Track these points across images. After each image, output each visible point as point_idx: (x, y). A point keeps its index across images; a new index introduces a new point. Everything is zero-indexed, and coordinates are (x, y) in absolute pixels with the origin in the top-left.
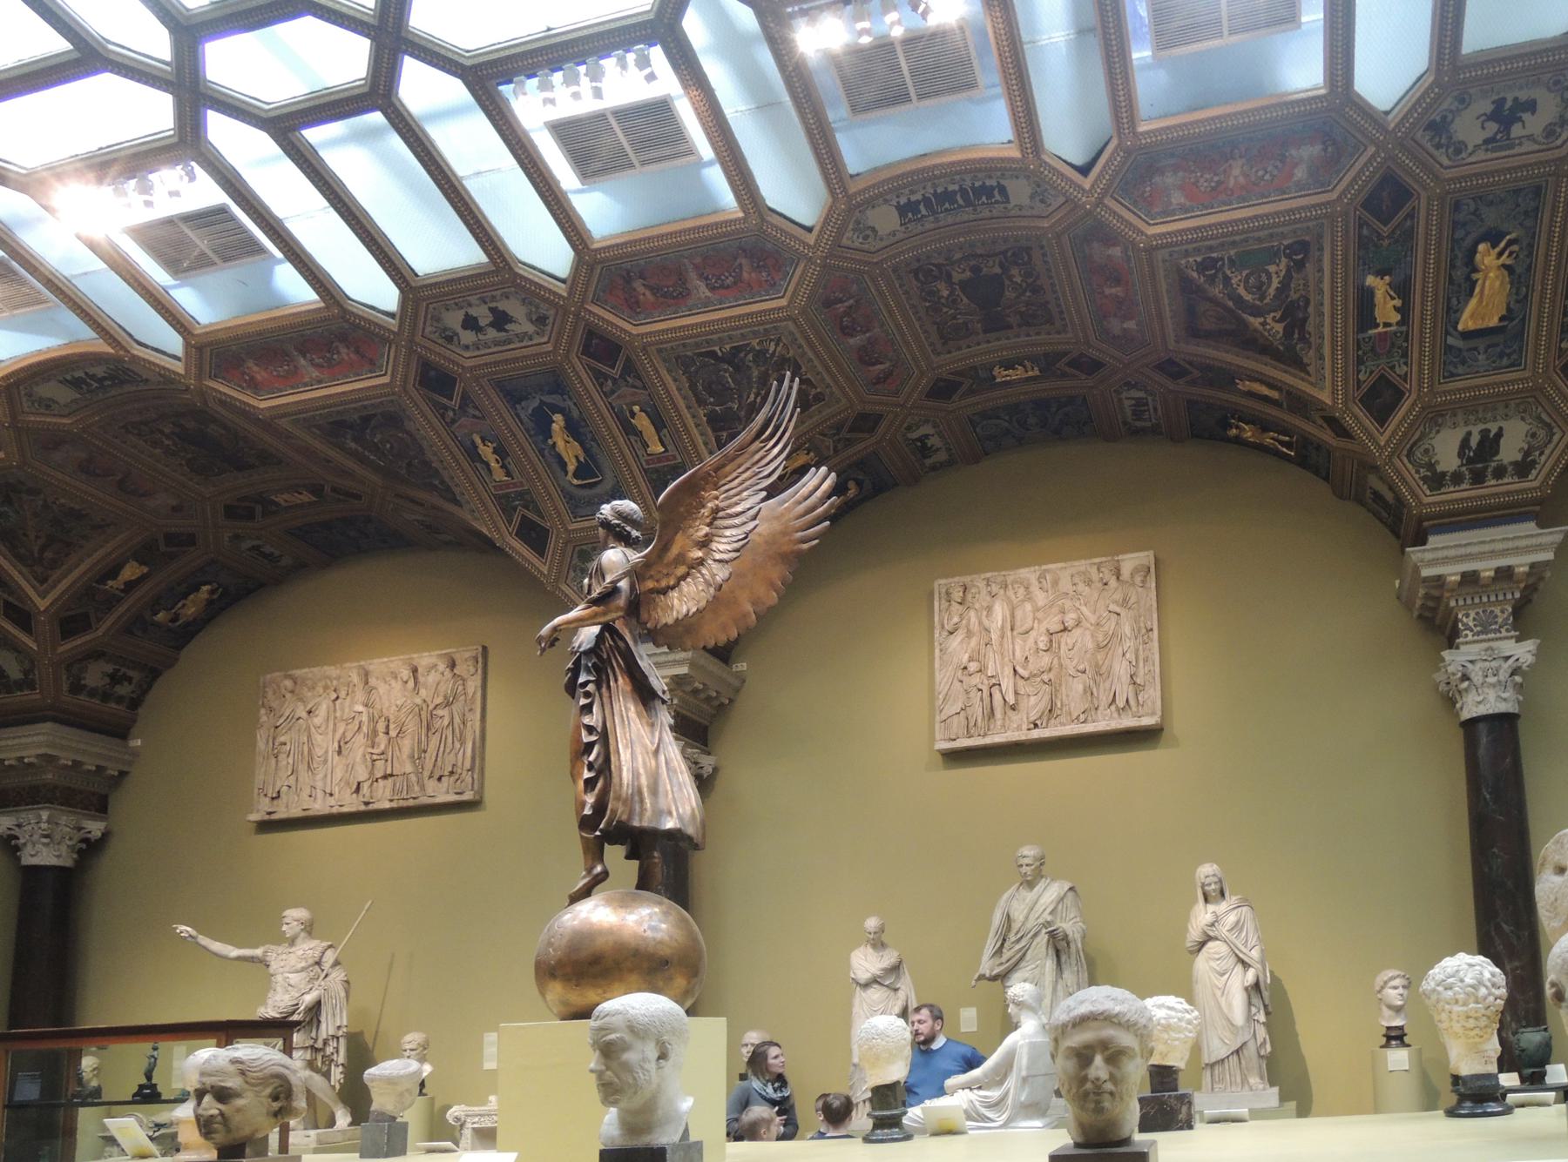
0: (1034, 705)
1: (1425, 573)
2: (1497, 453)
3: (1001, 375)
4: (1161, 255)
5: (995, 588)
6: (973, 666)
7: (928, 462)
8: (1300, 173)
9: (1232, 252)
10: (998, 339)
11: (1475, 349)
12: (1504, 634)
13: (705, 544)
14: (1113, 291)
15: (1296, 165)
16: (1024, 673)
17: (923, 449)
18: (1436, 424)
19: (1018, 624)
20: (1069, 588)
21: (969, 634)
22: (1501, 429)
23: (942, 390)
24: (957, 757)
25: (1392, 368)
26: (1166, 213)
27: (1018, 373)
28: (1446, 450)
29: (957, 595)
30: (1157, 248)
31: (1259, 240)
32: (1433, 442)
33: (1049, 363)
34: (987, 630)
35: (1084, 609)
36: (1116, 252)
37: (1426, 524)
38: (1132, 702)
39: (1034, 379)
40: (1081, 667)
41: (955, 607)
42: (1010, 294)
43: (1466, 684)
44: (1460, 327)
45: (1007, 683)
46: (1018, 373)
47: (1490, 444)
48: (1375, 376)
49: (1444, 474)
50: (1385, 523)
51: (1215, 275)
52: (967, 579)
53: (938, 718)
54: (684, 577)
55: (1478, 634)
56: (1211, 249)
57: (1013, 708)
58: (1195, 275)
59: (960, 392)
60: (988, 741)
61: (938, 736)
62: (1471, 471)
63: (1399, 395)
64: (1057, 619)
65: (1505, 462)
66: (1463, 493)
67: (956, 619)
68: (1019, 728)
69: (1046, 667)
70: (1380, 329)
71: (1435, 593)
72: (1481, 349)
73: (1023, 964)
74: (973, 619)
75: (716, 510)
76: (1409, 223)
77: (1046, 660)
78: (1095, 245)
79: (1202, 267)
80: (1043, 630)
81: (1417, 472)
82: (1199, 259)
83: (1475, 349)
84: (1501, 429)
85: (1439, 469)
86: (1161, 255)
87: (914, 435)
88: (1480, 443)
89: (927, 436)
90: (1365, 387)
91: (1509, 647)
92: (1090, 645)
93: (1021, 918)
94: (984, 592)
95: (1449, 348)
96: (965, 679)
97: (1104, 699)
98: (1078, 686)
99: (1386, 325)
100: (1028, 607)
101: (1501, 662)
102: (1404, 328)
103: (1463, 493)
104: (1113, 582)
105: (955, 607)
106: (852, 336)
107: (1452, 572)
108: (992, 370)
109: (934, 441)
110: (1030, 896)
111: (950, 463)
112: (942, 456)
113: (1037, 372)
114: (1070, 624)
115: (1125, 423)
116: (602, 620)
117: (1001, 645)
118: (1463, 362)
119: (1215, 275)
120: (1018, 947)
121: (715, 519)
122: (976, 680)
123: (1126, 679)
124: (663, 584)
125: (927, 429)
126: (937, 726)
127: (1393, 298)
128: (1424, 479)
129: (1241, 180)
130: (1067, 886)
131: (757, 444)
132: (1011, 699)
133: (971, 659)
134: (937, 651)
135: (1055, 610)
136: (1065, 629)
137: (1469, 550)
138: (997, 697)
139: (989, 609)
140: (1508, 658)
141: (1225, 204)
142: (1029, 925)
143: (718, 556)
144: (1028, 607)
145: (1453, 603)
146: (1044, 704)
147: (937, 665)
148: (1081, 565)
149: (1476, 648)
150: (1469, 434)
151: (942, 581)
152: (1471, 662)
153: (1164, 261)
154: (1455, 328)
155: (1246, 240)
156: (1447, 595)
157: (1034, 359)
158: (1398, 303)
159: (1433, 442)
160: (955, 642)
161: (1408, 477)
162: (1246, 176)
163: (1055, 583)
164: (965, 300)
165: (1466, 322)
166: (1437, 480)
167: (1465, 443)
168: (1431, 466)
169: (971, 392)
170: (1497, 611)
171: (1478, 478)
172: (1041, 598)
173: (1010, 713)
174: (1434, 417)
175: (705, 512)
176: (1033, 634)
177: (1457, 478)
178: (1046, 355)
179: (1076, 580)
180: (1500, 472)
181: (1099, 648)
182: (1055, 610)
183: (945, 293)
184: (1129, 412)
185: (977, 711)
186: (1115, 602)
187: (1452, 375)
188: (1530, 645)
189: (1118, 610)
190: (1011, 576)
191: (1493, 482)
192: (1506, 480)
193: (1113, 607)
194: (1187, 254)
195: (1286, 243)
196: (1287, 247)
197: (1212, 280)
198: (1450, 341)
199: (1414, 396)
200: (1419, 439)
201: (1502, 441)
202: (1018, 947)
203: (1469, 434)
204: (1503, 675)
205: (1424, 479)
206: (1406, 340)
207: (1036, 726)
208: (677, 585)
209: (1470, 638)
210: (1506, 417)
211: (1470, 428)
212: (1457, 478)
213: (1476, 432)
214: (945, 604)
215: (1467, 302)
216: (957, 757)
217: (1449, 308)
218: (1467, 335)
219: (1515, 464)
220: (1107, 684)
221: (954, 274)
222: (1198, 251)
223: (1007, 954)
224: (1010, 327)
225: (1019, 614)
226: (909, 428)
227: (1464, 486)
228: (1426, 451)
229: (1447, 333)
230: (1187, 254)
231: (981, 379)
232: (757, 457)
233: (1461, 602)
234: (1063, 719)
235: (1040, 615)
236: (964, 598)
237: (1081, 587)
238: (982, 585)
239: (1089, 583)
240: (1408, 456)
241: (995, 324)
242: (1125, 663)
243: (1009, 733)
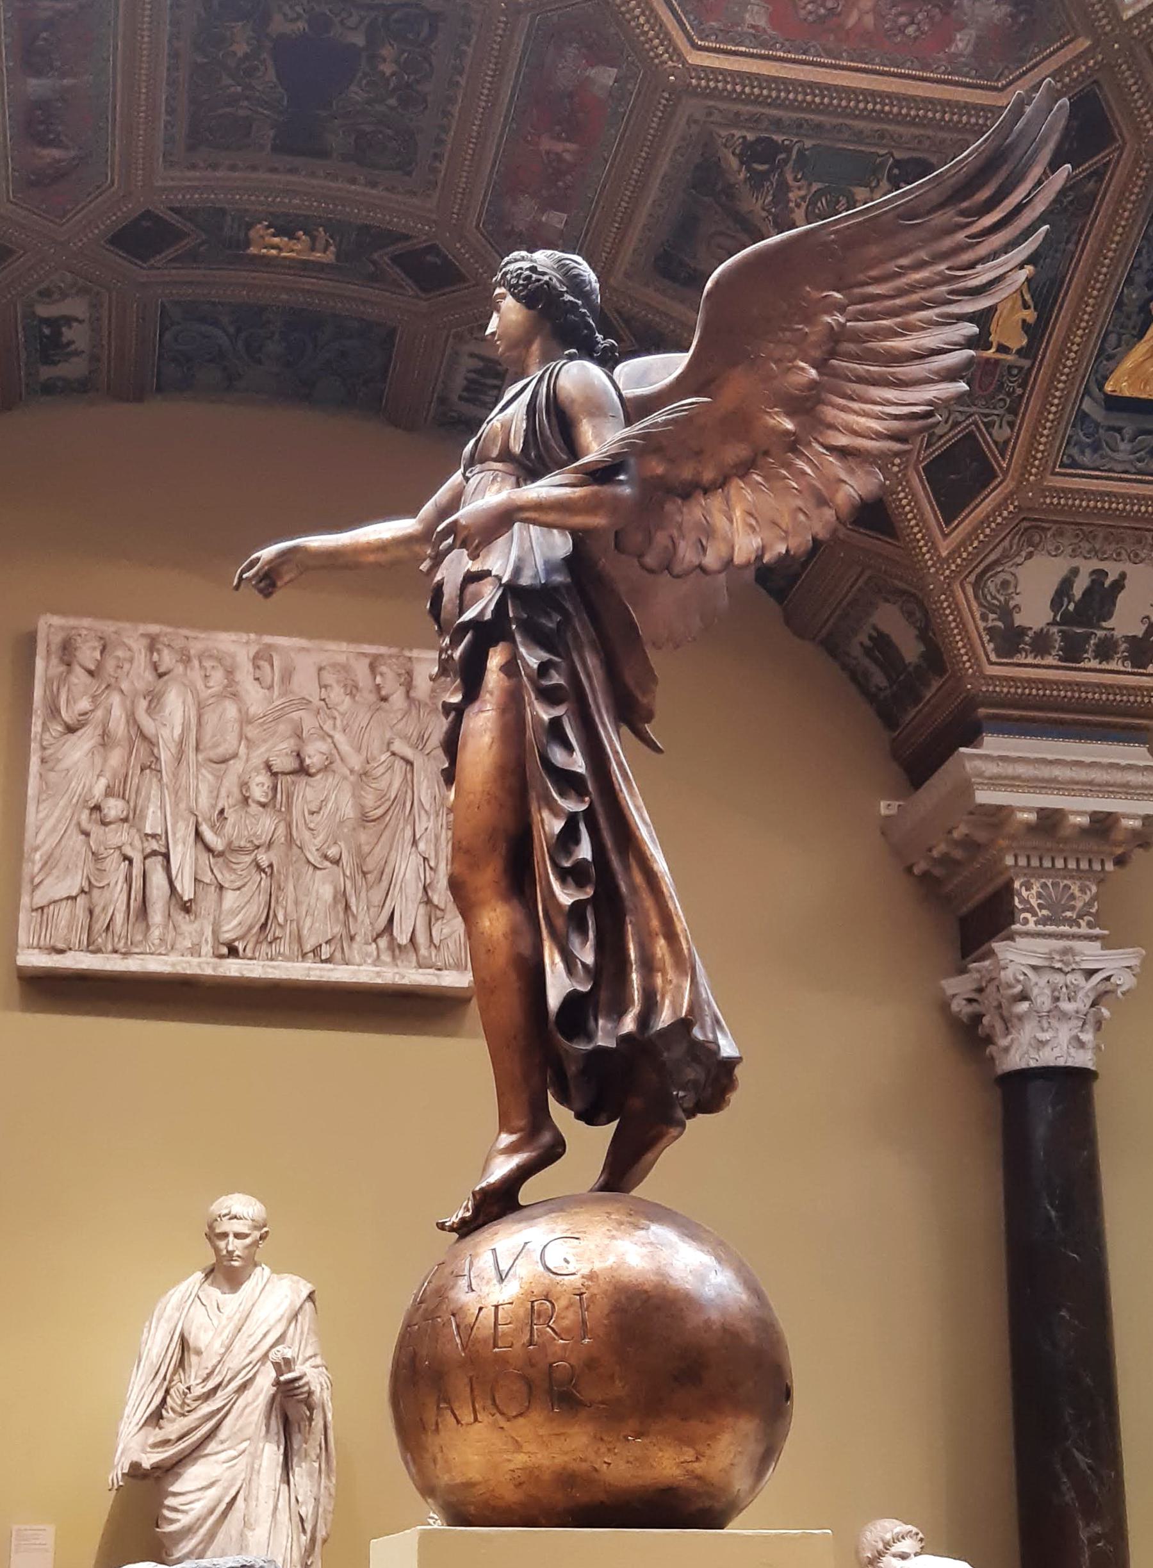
0: (237, 910)
1: (984, 797)
2: (1109, 615)
3: (268, 244)
4: (691, 107)
5: (167, 659)
6: (114, 808)
7: (46, 372)
8: (962, 43)
9: (808, 143)
10: (292, 171)
11: (1119, 430)
12: (1084, 930)
13: (805, 405)
14: (559, 147)
15: (962, 26)
16: (216, 842)
17: (50, 342)
18: (1030, 543)
19: (207, 740)
20: (311, 691)
21: (105, 740)
22: (1123, 576)
23: (142, 237)
24: (55, 990)
25: (989, 425)
26: (726, 34)
27: (295, 249)
28: (1035, 588)
29: (88, 654)
30: (694, 92)
31: (859, 136)
32: (1018, 571)
33: (361, 244)
34: (150, 742)
35: (339, 737)
36: (606, 76)
37: (982, 711)
38: (421, 939)
39: (320, 267)
40: (333, 852)
41: (79, 677)
42: (356, 93)
43: (1024, 1006)
44: (1108, 388)
45: (183, 855)
46: (295, 249)
47: (1102, 597)
48: (956, 434)
49: (1023, 631)
50: (871, 697)
51: (765, 175)
52: (108, 627)
53: (25, 900)
54: (744, 469)
55: (1044, 921)
56: (778, 124)
57: (186, 908)
58: (734, 162)
59: (170, 253)
60: (132, 965)
61: (22, 938)
62: (1065, 636)
63: (986, 476)
64: (288, 745)
65: (1118, 634)
66: (1044, 670)
67: (84, 704)
68: (195, 951)
69: (265, 839)
70: (990, 353)
71: (981, 836)
72: (1128, 431)
73: (212, 1446)
74: (117, 712)
75: (836, 336)
76: (1091, 185)
77: (266, 825)
78: (571, 51)
79: (753, 153)
80: (257, 760)
81: (984, 618)
82: (751, 137)
83: (1119, 430)
84: (1123, 576)
85: (1019, 620)
86: (691, 107)
87: (44, 310)
88: (1087, 593)
89: (68, 320)
90: (938, 449)
91: (1090, 953)
92: (348, 810)
93: (218, 1347)
94: (141, 658)
95: (1083, 417)
96: (96, 830)
97: (365, 921)
98: (322, 888)
99: (1002, 349)
100: (231, 710)
101: (1077, 979)
102: (1026, 363)
103: (1044, 670)
104: (398, 699)
105: (79, 677)
106: (38, 73)
107: (1026, 804)
108: (250, 226)
109: (77, 336)
110: (233, 1302)
111: (81, 388)
112: (72, 369)
113: (329, 257)
114: (313, 760)
115: (443, 400)
116: (579, 520)
117: (175, 775)
118: (1096, 448)
119: (765, 175)
120: (206, 1408)
121: (833, 354)
122: (119, 836)
123: (414, 891)
124: (687, 473)
125: (75, 307)
126: (23, 917)
127: (1026, 306)
128: (990, 630)
129: (869, 21)
130: (305, 1289)
131: (947, 216)
132: (186, 890)
133: (109, 792)
134: (34, 760)
135: (283, 728)
136: (302, 770)
137: (1057, 772)
138: (158, 879)
139: (154, 699)
140: (1090, 973)
141: (829, 54)
142: (235, 1361)
143: (842, 440)
144: (231, 710)
145: (1009, 861)
146: (254, 911)
147: (32, 791)
148: (339, 651)
149: (1044, 946)
150: (1075, 572)
151: (56, 620)
152: (1035, 968)
153: (691, 121)
154: (1101, 387)
155: (838, 128)
156: (1003, 843)
157: (336, 229)
158: (1030, 315)
159: (1018, 571)
160: (78, 751)
161: (968, 621)
162: (879, 16)
163: (287, 676)
164: (271, 75)
165: (1120, 384)
166: (1010, 640)
167: (1064, 589)
168: (1006, 613)
169: (192, 257)
170: (1075, 889)
171: (1072, 653)
172: (255, 697)
173: (179, 917)
174: (1032, 528)
175: (813, 333)
176: (236, 766)
177: (1041, 644)
178: (365, 229)
179: (329, 678)
180: (1105, 650)
181: (364, 819)
182: (283, 728)
183: (242, 49)
184: (459, 382)
185: (115, 899)
186: (406, 738)
187: (1074, 464)
188: (1129, 957)
189: (409, 753)
190: (200, 641)
191: (1094, 664)
192: (1112, 666)
193: (399, 746)
194: (736, 120)
195: (898, 155)
196: (898, 163)
197: (757, 181)
198: (1087, 405)
199: (1010, 484)
200: (997, 562)
201: (1121, 596)
202: (206, 1408)
203: (1075, 572)
204: (1081, 1004)
205: (990, 630)
206: (1023, 385)
207: (233, 952)
208: (722, 483)
209: (1031, 926)
210: (1135, 559)
211: (1077, 562)
212: (1041, 644)
213: (1087, 567)
214: (57, 669)
215: (1130, 347)
216: (55, 990)
217: (1102, 350)
218: (1115, 403)
219: (1132, 640)
220: (377, 896)
221: (278, 17)
222: (754, 121)
223: (173, 1427)
224: (323, 154)
225: (211, 719)
226: (46, 294)
227: (1050, 660)
228: (1005, 584)
229: (1087, 392)
230: (736, 120)
231: (221, 236)
232: (947, 243)
233: (1022, 862)
234: (284, 947)
235: (251, 731)
236: (100, 665)
237: (337, 694)
238: (139, 647)
239: (352, 689)
240: (976, 585)
241: (299, 141)
242: (415, 860)
243: (173, 958)
